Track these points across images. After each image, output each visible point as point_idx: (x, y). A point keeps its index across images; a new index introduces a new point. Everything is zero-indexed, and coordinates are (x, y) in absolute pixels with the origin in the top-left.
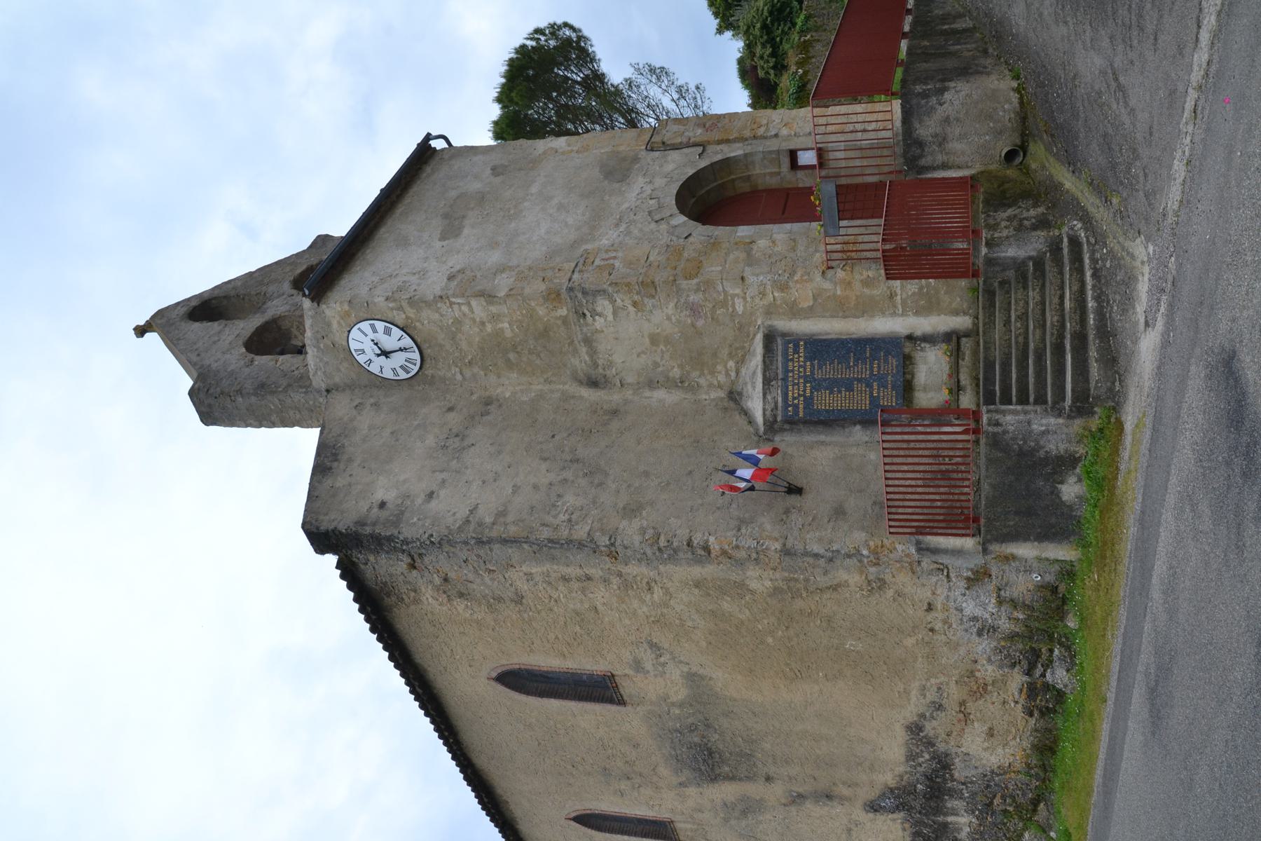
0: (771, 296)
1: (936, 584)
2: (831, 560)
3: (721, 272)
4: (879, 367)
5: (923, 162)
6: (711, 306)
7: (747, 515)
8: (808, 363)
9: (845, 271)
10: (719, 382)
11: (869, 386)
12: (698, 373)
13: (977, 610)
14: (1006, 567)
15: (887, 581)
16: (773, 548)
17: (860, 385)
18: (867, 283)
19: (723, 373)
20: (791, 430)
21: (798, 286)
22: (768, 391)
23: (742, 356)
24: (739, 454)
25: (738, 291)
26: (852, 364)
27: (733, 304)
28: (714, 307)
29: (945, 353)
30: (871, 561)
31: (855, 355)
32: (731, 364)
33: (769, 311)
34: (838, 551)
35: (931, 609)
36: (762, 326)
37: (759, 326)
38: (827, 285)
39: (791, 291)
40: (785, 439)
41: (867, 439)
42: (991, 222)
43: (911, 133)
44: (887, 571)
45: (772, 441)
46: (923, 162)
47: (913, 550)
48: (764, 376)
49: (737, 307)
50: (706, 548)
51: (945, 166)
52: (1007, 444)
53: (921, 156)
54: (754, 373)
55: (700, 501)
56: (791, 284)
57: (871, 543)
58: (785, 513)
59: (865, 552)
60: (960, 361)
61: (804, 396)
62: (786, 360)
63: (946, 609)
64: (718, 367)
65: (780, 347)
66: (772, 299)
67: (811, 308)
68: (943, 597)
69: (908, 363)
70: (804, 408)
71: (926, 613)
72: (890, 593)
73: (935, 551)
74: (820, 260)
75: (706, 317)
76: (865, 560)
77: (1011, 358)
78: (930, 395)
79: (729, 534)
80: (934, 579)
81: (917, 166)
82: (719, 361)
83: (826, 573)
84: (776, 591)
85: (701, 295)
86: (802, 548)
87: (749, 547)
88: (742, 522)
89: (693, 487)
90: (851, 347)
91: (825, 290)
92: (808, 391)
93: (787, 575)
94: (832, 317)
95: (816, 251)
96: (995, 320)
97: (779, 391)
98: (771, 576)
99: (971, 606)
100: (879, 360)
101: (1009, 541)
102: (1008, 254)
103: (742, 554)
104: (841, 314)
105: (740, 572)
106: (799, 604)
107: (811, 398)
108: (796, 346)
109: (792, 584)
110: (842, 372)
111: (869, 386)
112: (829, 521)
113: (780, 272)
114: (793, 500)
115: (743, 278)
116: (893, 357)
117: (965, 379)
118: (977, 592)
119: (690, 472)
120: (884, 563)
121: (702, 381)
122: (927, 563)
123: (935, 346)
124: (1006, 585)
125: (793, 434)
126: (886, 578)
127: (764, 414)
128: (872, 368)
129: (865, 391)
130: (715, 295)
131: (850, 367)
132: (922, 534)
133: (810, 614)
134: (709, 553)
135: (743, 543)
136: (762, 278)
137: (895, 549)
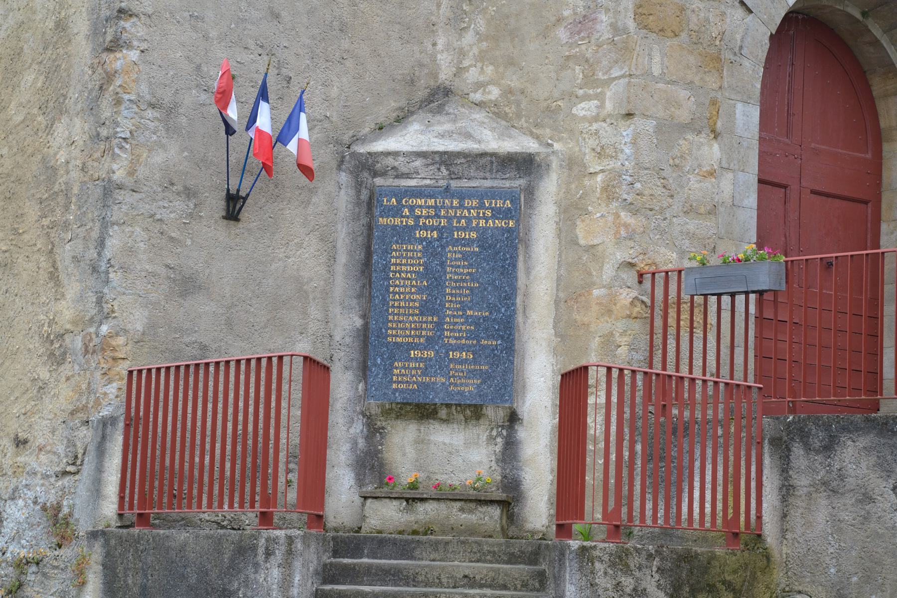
0: (599, 168)
1: (55, 453)
2: (95, 269)
3: (648, 74)
4: (462, 362)
5: (798, 450)
6: (588, 55)
7: (183, 120)
8: (474, 235)
9: (632, 303)
10: (466, 69)
11: (430, 342)
12: (483, 29)
13: (11, 525)
14: (69, 574)
15: (61, 369)
16: (115, 167)
17: (430, 326)
18: (609, 342)
19: (482, 78)
20: (358, 203)
21: (610, 218)
22: (430, 161)
23: (506, 114)
24: (300, 106)
25: (609, 106)
26: (469, 313)
27: (587, 98)
28: (587, 61)
29: (479, 479)
30: (91, 340)
31: (485, 319)
32: (494, 93)
33: (573, 164)
34: (107, 282)
35: (17, 446)
36: (549, 150)
37: (551, 145)
38: (608, 271)
39: (603, 205)
40: (343, 192)
41: (337, 338)
42: (633, 562)
43: (850, 432)
44: (77, 367)
45: (339, 167)
46: (798, 450)
47: (105, 412)
48: (459, 154)
49: (582, 105)
50: (114, 46)
51: (787, 491)
52: (240, 571)
53: (808, 448)
54: (468, 136)
55: (213, 34)
56: (615, 204)
57: (121, 340)
58: (186, 188)
59: (104, 329)
60: (458, 504)
61: (416, 226)
62: (482, 195)
63: (18, 470)
64: (491, 68)
65: (507, 184)
66: (592, 170)
67: (574, 242)
68: (34, 465)
69: (468, 412)
70: (394, 227)
71: (12, 436)
72: (44, 373)
73: (101, 451)
74: (658, 259)
75: (571, 46)
76: (92, 330)
77: (408, 585)
78: (411, 452)
79: (144, 88)
80: (61, 449)
81: (792, 439)
82: (501, 70)
83: (76, 259)
84: (51, 171)
85: (607, 35)
86: (114, 219)
87: (117, 124)
88: (169, 112)
89: (244, 20)
90: (499, 311)
91: (601, 268)
92: (424, 234)
93: (76, 190)
94: (559, 279)
95: (682, 253)
96: (485, 561)
97: (428, 182)
98: (73, 162)
99: (18, 514)
100: (475, 361)
101: (105, 576)
102: (568, 586)
103: (106, 113)
104: (562, 295)
105: (79, 106)
106: (32, 211)
107: (411, 240)
108: (506, 214)
109: (61, 199)
110: (455, 295)
111: (430, 342)
112: (168, 266)
113: (638, 185)
114: (216, 204)
115: (629, 115)
116: (479, 386)
117: (427, 511)
118: (39, 524)
119: (276, 16)
120: (88, 362)
121: (469, 38)
122: (85, 435)
123: (497, 461)
124: (45, 575)
125: (350, 206)
126: (67, 366)
127: (388, 154)
128: (460, 348)
129: (420, 336)
130: (605, 63)
131: (464, 310)
132: (127, 426)
133: (15, 231)
134: (109, 50)
135: (125, 113)
136: (627, 151)
137: (110, 381)
